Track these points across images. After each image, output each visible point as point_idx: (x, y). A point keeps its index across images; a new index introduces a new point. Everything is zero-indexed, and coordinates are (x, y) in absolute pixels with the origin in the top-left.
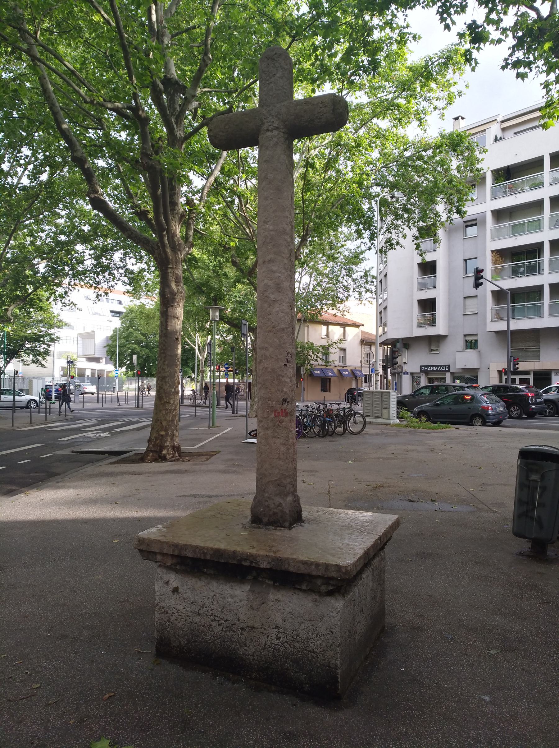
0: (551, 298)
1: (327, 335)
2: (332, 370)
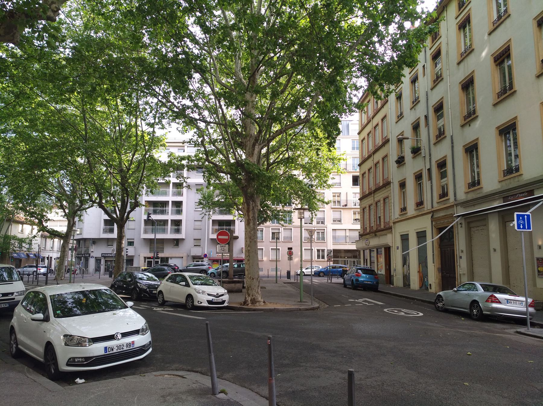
0: (171, 226)
1: (22, 231)
2: (23, 254)
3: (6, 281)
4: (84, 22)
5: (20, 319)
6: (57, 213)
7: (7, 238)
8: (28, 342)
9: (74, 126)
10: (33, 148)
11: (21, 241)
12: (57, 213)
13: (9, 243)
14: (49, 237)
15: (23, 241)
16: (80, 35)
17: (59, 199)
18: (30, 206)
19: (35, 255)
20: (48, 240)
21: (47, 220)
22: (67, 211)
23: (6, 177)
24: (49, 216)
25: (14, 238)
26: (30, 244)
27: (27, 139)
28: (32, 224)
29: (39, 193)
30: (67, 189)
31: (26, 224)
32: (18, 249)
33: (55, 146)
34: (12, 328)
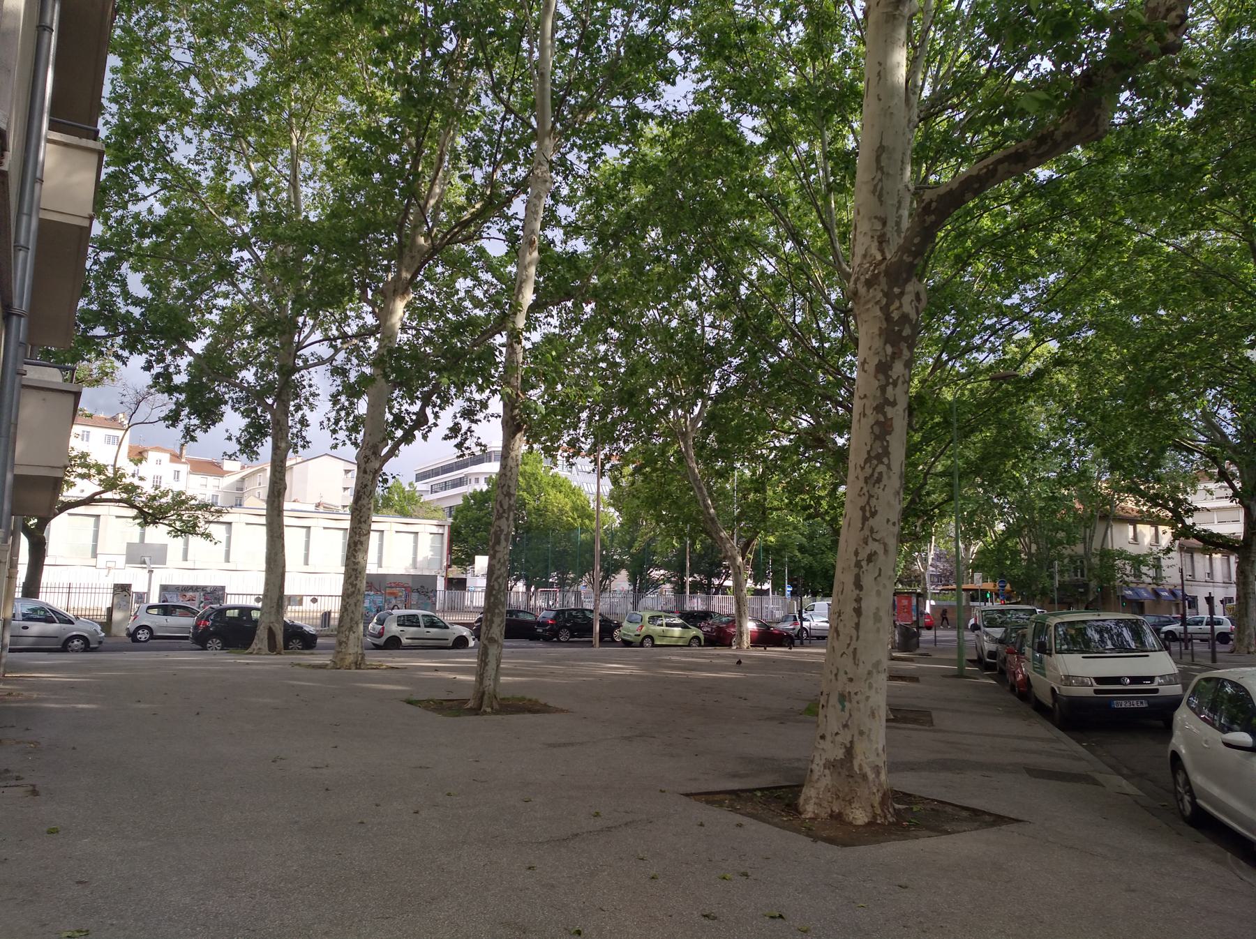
1: (1135, 538)
3: (1132, 650)
4: (1220, 17)
5: (1189, 739)
6: (1210, 492)
7: (1107, 556)
8: (1216, 791)
9: (1229, 274)
10: (1139, 350)
11: (1137, 561)
12: (1210, 492)
13: (1113, 566)
14: (1204, 551)
15: (1141, 562)
16: (1214, 53)
17: (1212, 458)
18: (1149, 482)
19: (1173, 593)
20: (1197, 557)
21: (1192, 510)
22: (1238, 485)
23: (1089, 424)
24: (1197, 500)
25: (1122, 554)
26: (1158, 567)
27: (1121, 333)
28: (1155, 522)
29: (1163, 450)
30: (1230, 430)
31: (1142, 522)
32: (1131, 578)
33: (1189, 333)
34: (1175, 756)
